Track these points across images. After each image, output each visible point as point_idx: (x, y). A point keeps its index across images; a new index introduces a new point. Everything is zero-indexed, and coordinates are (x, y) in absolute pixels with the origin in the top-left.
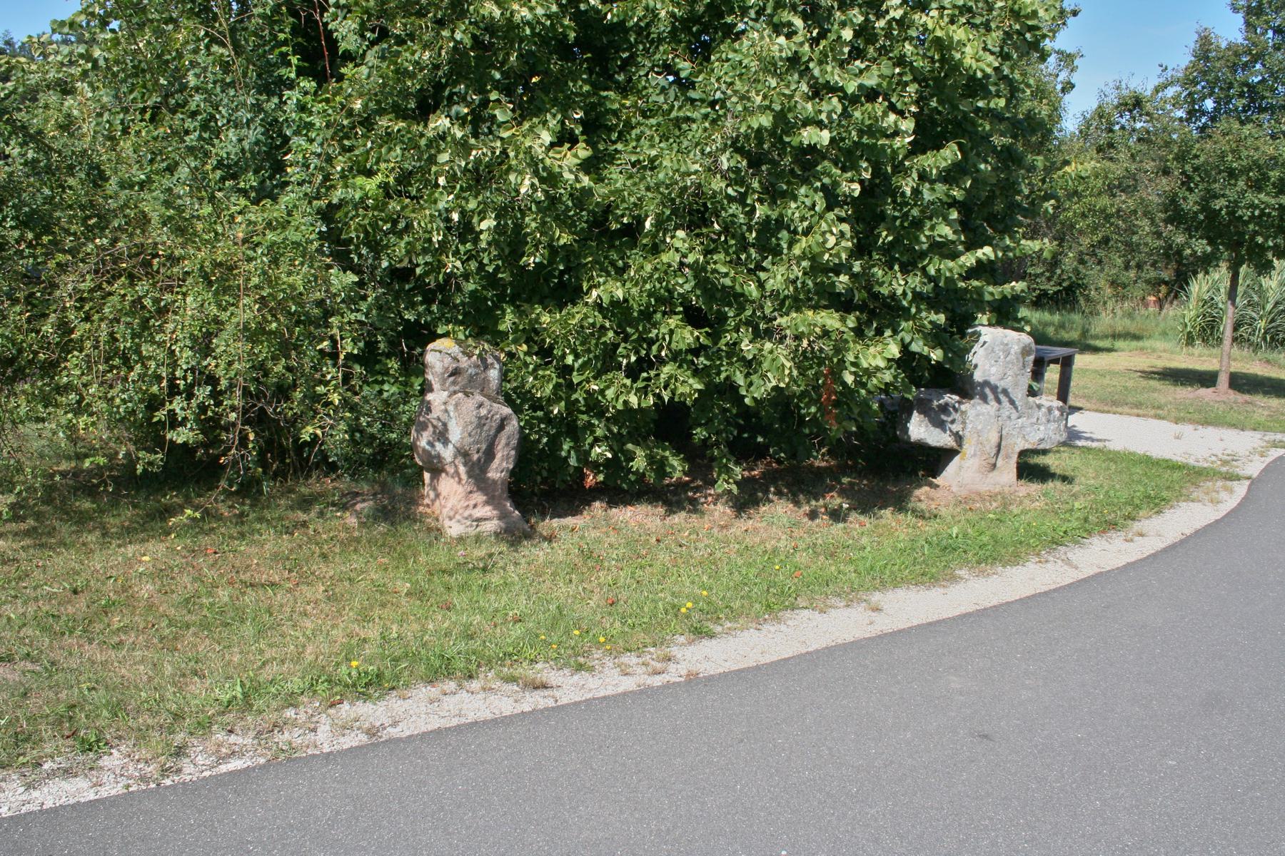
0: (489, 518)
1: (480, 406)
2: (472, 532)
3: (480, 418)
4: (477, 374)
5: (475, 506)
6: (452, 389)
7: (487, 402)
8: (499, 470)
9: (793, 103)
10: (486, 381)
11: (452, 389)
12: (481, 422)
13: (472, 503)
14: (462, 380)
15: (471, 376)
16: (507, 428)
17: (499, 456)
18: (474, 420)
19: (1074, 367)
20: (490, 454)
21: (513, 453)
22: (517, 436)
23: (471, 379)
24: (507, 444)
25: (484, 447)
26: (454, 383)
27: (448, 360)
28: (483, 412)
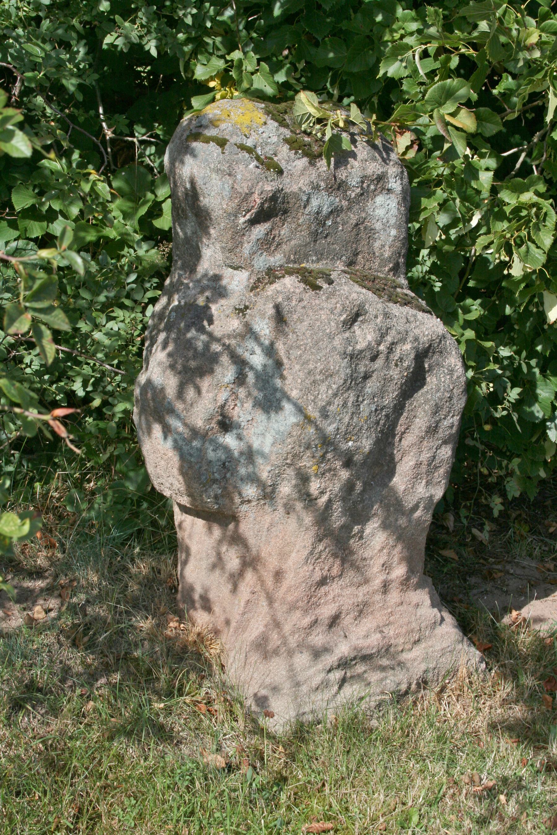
1: (355, 317)
3: (354, 357)
4: (335, 212)
7: (374, 304)
9: (459, 163)
10: (362, 230)
11: (263, 261)
14: (291, 232)
15: (319, 220)
16: (431, 380)
18: (341, 367)
19: (196, 519)
21: (446, 452)
22: (460, 404)
23: (320, 227)
24: (432, 430)
26: (268, 244)
27: (248, 169)
28: (364, 336)
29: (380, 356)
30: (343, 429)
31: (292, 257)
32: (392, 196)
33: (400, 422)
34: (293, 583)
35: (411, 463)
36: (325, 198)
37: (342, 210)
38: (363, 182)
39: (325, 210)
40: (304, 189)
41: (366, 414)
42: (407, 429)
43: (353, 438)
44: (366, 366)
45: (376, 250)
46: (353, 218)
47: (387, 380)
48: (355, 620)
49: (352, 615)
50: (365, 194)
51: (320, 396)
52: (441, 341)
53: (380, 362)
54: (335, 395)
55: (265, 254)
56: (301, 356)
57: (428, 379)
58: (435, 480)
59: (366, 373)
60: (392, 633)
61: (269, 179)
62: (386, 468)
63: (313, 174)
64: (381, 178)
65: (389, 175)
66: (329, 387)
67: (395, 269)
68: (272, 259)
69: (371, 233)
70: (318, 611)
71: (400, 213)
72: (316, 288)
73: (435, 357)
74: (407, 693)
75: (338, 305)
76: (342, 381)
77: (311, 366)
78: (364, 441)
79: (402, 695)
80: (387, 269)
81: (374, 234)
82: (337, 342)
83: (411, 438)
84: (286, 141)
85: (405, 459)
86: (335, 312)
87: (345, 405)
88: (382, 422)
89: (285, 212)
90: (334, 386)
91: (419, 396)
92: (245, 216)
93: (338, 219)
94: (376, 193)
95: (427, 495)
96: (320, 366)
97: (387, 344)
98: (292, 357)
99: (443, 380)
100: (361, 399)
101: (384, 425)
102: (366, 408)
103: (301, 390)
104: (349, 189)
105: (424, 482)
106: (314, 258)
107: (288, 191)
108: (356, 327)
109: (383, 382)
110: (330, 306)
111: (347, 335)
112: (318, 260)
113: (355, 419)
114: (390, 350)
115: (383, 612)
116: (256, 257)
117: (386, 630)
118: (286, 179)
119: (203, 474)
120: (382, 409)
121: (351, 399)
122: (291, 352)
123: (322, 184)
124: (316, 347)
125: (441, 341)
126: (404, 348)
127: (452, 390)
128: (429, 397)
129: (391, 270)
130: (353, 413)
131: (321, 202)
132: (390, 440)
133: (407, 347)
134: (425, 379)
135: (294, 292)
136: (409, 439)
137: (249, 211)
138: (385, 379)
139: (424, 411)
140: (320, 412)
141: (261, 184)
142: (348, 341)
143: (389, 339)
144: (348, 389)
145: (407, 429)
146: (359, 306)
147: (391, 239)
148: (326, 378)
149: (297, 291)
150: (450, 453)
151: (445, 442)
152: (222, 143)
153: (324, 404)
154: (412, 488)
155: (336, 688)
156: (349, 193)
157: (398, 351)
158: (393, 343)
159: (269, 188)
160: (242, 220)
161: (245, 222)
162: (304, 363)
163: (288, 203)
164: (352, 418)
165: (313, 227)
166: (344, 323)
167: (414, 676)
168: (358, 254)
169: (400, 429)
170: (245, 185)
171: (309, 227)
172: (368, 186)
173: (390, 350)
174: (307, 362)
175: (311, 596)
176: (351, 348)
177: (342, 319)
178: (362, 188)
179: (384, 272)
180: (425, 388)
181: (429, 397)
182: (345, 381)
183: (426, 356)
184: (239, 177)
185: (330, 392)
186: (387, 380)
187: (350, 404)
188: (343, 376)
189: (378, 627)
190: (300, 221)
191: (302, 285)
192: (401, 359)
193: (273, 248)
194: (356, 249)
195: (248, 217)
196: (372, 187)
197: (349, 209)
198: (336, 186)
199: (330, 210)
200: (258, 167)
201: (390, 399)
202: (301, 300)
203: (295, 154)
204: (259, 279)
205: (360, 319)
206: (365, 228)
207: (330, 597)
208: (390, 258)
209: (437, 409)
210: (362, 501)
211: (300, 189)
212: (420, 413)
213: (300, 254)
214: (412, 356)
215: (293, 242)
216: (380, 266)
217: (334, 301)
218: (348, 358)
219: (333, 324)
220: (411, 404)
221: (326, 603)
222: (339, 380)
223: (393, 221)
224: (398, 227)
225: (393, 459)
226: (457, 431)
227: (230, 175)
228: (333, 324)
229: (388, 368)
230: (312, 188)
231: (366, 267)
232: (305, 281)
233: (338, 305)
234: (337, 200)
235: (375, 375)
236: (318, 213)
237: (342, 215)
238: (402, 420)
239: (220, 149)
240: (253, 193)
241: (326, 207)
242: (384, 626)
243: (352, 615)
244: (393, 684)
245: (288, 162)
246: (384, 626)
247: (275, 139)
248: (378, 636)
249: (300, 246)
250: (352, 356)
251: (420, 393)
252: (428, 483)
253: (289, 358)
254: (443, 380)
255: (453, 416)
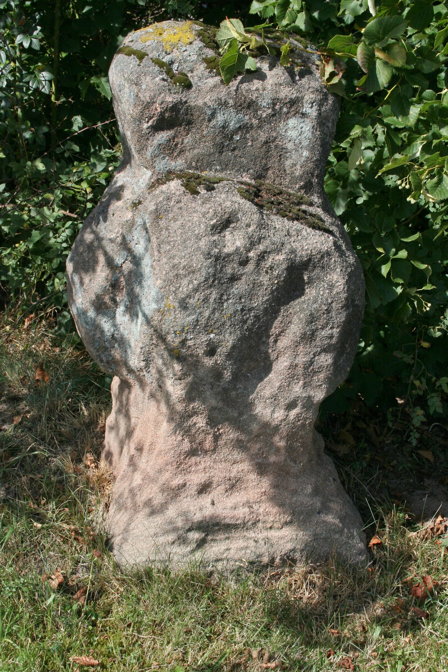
0: (262, 525)
1: (225, 223)
2: (182, 560)
3: (220, 260)
4: (244, 128)
5: (204, 489)
6: (162, 164)
8: (287, 391)
10: (272, 148)
11: (162, 164)
12: (221, 273)
13: (196, 479)
14: (195, 143)
16: (310, 293)
17: (281, 365)
20: (253, 356)
21: (326, 360)
23: (226, 141)
24: (308, 337)
25: (229, 340)
26: (170, 149)
28: (234, 241)
29: (251, 261)
30: (203, 321)
31: (194, 164)
32: (307, 120)
33: (274, 325)
34: (163, 448)
35: (286, 364)
36: (233, 115)
37: (252, 127)
38: (274, 104)
39: (232, 125)
40: (209, 104)
41: (231, 311)
42: (282, 332)
43: (215, 331)
44: (234, 268)
45: (287, 168)
46: (263, 136)
47: (255, 285)
48: (226, 491)
49: (223, 487)
50: (276, 115)
51: (181, 289)
52: (322, 257)
53: (250, 267)
54: (196, 290)
55: (167, 158)
56: (169, 251)
57: (307, 291)
58: (314, 384)
59: (233, 274)
60: (261, 510)
61: (172, 91)
62: (262, 364)
63: (223, 92)
64: (294, 103)
65: (305, 100)
66: (191, 282)
67: (308, 187)
68: (173, 163)
69: (283, 153)
70: (188, 477)
71: (315, 137)
72: (195, 192)
73: (317, 271)
74: (266, 566)
75: (211, 210)
76: (203, 279)
77: (176, 261)
78: (227, 335)
79: (263, 566)
80: (297, 186)
81: (286, 153)
82: (203, 243)
83: (286, 341)
84: (205, 60)
85: (281, 359)
86: (207, 216)
87: (206, 300)
88: (249, 322)
89: (189, 123)
90: (195, 282)
91: (296, 305)
92: (148, 122)
93: (248, 136)
94: (289, 115)
95: (304, 395)
96: (184, 263)
97: (258, 252)
98: (162, 251)
99: (321, 293)
100: (225, 297)
101: (253, 324)
102: (230, 307)
103: (165, 281)
104: (260, 109)
105: (301, 383)
106: (218, 167)
107: (192, 104)
108: (227, 233)
109: (251, 286)
110: (204, 210)
111: (215, 238)
112: (222, 170)
113: (217, 315)
114: (262, 257)
115: (256, 491)
116: (158, 160)
117: (255, 507)
118: (192, 94)
119: (97, 342)
120: (250, 310)
121: (213, 296)
122: (162, 246)
123: (231, 102)
124: (184, 245)
125: (322, 257)
126: (277, 258)
127: (330, 304)
128: (305, 306)
129: (301, 188)
130: (214, 309)
131: (230, 118)
132: (264, 339)
133: (281, 257)
134: (304, 290)
135: (174, 194)
136: (284, 342)
137: (151, 118)
138: (254, 283)
139: (299, 319)
140: (179, 303)
141: (163, 95)
142: (215, 244)
143: (261, 247)
144: (211, 286)
145: (282, 332)
146: (231, 213)
147: (303, 159)
148: (189, 274)
149: (178, 193)
150: (330, 361)
151: (325, 350)
152: (141, 56)
153: (183, 296)
154: (288, 386)
155: (194, 546)
156: (259, 113)
157: (270, 260)
158: (265, 252)
159: (170, 99)
160: (145, 126)
161: (148, 128)
162: (171, 258)
163: (192, 115)
164: (213, 312)
165: (218, 139)
166: (214, 227)
167: (278, 552)
168: (268, 169)
169: (274, 331)
170: (147, 94)
171: (214, 139)
172: (281, 108)
173: (262, 257)
174: (173, 257)
175: (181, 464)
176: (217, 250)
177: (212, 223)
178: (273, 109)
179: (294, 190)
180: (303, 298)
181: (305, 306)
182: (206, 280)
183: (306, 269)
184: (144, 87)
185: (191, 286)
186: (255, 285)
187: (211, 300)
188: (204, 274)
189: (248, 502)
190: (204, 133)
191: (183, 189)
192: (271, 268)
193: (175, 154)
194: (266, 165)
195: (150, 123)
196: (285, 110)
197: (260, 127)
198: (245, 105)
199: (237, 126)
200: (163, 80)
201: (260, 301)
202: (179, 202)
203: (210, 72)
204: (158, 179)
205: (232, 225)
206: (276, 147)
207: (201, 467)
208: (301, 177)
209: (312, 319)
210: (235, 389)
211: (205, 104)
212: (295, 319)
213: (202, 163)
214: (284, 266)
215: (196, 151)
216: (291, 182)
217: (208, 206)
218: (213, 258)
219: (202, 226)
220: (287, 310)
221: (196, 472)
222: (199, 278)
223: (305, 143)
224: (312, 149)
225: (269, 357)
226: (337, 343)
227: (136, 84)
228: (202, 226)
229: (259, 274)
230: (219, 104)
231: (276, 182)
232: (186, 186)
233: (211, 210)
234: (247, 117)
235: (244, 278)
236: (223, 127)
237: (253, 132)
238: (276, 323)
239: (138, 62)
240: (154, 102)
241: (233, 122)
242: (255, 503)
243: (223, 487)
244: (253, 554)
245: (200, 79)
246: (255, 503)
247: (194, 58)
248: (247, 510)
249: (203, 155)
250: (217, 258)
251: (297, 301)
252: (305, 386)
253: (159, 252)
254: (321, 293)
255: (331, 328)
